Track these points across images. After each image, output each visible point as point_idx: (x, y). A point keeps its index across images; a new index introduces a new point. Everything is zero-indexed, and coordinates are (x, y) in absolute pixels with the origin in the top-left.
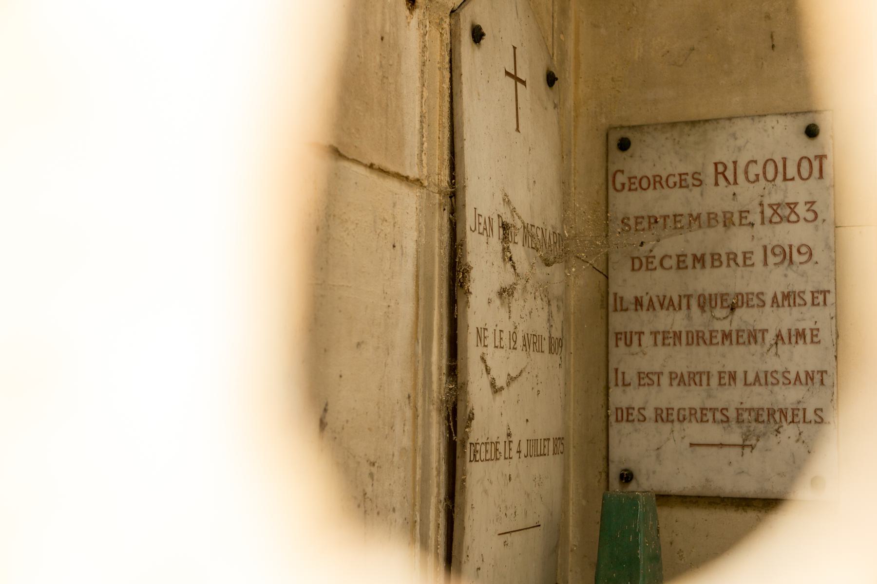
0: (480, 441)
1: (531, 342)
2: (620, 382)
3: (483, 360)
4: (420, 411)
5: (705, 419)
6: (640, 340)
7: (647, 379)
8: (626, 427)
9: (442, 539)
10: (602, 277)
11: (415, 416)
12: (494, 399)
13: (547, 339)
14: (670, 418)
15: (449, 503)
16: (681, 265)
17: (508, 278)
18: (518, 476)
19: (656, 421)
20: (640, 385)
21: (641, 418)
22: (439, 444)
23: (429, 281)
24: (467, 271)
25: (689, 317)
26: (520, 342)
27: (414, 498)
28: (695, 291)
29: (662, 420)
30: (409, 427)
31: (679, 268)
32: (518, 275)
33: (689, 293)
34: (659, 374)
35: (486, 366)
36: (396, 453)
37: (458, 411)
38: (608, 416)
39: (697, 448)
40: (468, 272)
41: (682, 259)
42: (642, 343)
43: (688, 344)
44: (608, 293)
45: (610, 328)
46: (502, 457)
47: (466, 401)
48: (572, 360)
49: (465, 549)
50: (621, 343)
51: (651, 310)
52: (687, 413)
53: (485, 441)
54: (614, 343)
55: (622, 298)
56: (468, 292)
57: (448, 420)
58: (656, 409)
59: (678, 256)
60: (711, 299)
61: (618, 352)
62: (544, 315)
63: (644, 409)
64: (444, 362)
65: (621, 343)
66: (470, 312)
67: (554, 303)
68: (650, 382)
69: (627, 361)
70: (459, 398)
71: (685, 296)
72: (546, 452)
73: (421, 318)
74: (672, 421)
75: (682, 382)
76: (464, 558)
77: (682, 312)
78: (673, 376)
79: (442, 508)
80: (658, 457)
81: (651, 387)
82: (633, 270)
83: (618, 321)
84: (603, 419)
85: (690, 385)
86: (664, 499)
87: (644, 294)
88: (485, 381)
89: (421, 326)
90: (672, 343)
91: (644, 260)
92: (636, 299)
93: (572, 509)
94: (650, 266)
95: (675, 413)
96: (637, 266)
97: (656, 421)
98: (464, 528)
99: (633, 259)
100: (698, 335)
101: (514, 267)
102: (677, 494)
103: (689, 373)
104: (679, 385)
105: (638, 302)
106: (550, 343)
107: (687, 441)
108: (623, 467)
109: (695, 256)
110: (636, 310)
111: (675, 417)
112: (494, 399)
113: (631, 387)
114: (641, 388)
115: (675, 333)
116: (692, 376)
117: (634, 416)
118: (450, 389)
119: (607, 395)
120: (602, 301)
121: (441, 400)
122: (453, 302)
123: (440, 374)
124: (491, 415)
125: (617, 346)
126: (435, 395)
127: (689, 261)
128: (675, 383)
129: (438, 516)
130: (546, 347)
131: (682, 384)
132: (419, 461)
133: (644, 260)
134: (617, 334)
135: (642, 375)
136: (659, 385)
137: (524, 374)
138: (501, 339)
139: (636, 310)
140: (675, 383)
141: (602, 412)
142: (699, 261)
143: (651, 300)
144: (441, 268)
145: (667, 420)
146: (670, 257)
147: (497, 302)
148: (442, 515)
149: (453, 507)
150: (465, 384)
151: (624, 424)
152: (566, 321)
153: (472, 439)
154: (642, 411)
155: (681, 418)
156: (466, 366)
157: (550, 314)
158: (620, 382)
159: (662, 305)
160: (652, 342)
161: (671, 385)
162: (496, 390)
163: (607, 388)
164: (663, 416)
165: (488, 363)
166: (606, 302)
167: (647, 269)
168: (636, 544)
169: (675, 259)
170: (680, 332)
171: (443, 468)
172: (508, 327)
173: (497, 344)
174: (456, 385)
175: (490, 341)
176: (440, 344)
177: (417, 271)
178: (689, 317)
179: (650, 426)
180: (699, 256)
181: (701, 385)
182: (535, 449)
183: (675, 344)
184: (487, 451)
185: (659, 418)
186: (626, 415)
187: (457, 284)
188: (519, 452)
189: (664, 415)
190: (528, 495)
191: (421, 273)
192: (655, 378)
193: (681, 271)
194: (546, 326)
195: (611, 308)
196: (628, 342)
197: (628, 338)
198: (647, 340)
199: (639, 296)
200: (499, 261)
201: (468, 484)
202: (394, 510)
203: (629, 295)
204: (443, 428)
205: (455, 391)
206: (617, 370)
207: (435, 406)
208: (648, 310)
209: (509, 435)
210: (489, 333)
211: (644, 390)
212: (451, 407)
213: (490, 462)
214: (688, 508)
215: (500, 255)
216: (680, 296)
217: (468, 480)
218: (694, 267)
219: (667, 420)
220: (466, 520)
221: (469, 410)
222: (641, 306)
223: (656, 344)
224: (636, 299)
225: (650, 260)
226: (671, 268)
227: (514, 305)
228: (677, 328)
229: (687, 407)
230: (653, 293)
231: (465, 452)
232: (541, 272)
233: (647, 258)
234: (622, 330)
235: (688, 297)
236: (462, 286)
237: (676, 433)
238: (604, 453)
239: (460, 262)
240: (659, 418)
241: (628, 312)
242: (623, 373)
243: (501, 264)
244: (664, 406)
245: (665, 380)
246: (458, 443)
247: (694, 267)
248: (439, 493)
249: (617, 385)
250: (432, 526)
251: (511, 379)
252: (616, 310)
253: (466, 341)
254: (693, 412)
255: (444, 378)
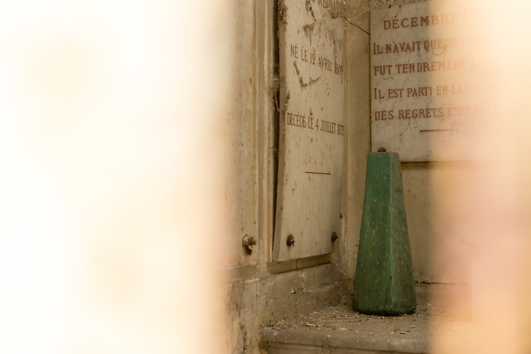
0: (294, 113)
1: (323, 63)
2: (378, 97)
3: (295, 64)
4: (257, 90)
5: (429, 115)
6: (389, 71)
7: (394, 93)
8: (382, 123)
9: (272, 171)
10: (367, 35)
11: (255, 93)
12: (302, 90)
13: (333, 64)
14: (408, 116)
15: (275, 149)
16: (414, 24)
17: (310, 21)
18: (317, 140)
19: (400, 118)
20: (389, 97)
21: (391, 117)
22: (269, 113)
23: (262, 15)
24: (284, 10)
25: (419, 55)
26: (317, 61)
27: (255, 141)
28: (423, 39)
29: (403, 117)
30: (250, 98)
31: (413, 26)
32: (315, 20)
33: (419, 40)
34: (401, 90)
35: (297, 69)
36: (243, 112)
37: (280, 94)
38: (370, 117)
39: (424, 133)
40: (285, 10)
41: (414, 20)
42: (391, 72)
43: (418, 71)
44: (370, 43)
45: (372, 64)
46: (307, 127)
47: (285, 88)
48: (349, 85)
49: (285, 176)
50: (378, 73)
51: (396, 52)
52: (418, 112)
53: (296, 114)
54: (374, 73)
55: (378, 46)
56: (285, 23)
57: (275, 100)
58: (400, 111)
59: (412, 19)
60: (432, 44)
61: (376, 78)
62: (332, 49)
63: (392, 111)
64: (272, 65)
65: (378, 73)
66: (287, 35)
67: (337, 44)
68: (396, 95)
69: (382, 83)
70: (281, 86)
71: (416, 42)
72: (333, 131)
73: (257, 34)
74: (409, 118)
75: (415, 94)
76: (285, 181)
77: (414, 52)
78: (410, 90)
79: (271, 151)
80: (401, 139)
81: (396, 98)
82: (385, 28)
83: (376, 60)
84: (368, 119)
85: (420, 95)
86: (406, 164)
87: (392, 43)
88: (296, 79)
89: (257, 40)
90: (409, 71)
91: (392, 22)
92: (387, 46)
93: (349, 174)
94: (395, 26)
95: (411, 113)
96: (387, 26)
97: (400, 118)
98: (285, 163)
99: (385, 22)
100: (424, 65)
101: (313, 14)
102: (412, 161)
103: (419, 88)
104: (413, 96)
105: (388, 48)
106: (335, 67)
107: (418, 129)
108: (380, 147)
109: (422, 18)
110: (387, 52)
111: (411, 115)
112: (302, 90)
113: (384, 99)
114: (390, 99)
115: (410, 65)
116: (421, 90)
117: (386, 116)
118: (276, 81)
119: (370, 105)
120: (367, 49)
121: (270, 88)
122: (276, 29)
123: (269, 72)
124: (299, 100)
125: (376, 75)
126: (266, 84)
127: (419, 21)
128: (411, 95)
129: (269, 156)
130: (333, 68)
131: (415, 95)
132: (257, 120)
133: (392, 22)
134: (375, 67)
135: (391, 91)
136: (401, 96)
137: (319, 80)
138: (306, 56)
139: (387, 52)
140: (411, 95)
141: (367, 115)
142: (425, 22)
143: (396, 46)
144: (269, 8)
145: (406, 118)
146: (408, 19)
147: (303, 33)
148: (272, 156)
149: (278, 151)
150: (284, 78)
151: (380, 121)
152: (345, 58)
153: (289, 111)
154: (391, 113)
155: (415, 115)
156: (285, 67)
157: (335, 50)
158: (378, 97)
159: (402, 49)
160: (397, 71)
161: (408, 96)
162: (303, 85)
163: (370, 100)
164: (404, 115)
165: (298, 67)
166: (369, 49)
167: (394, 27)
168: (388, 181)
169: (410, 20)
170: (414, 64)
171: (272, 129)
172: (310, 51)
173: (304, 58)
174: (279, 78)
175: (299, 55)
176: (269, 54)
177: (255, 6)
178: (419, 55)
179: (396, 121)
180: (425, 18)
181: (426, 95)
182: (327, 127)
183: (410, 72)
184: (298, 120)
185: (401, 116)
186: (382, 116)
187: (279, 18)
188: (317, 126)
189: (404, 115)
190: (323, 153)
191: (257, 8)
192: (399, 93)
193: (414, 28)
194: (333, 56)
195: (372, 52)
196: (382, 72)
197: (382, 70)
198: (394, 70)
199: (389, 44)
200: (304, 9)
201: (287, 137)
202: (242, 145)
203: (382, 44)
204: (272, 105)
205: (279, 82)
206: (375, 89)
207: (266, 91)
208: (394, 52)
209: (311, 114)
210: (299, 50)
211: (392, 100)
212: (276, 91)
213: (300, 127)
214: (419, 169)
215: (304, 5)
216: (413, 43)
217: (287, 134)
218: (422, 25)
219: (406, 118)
220: (286, 158)
221: (287, 93)
222: (390, 49)
223: (399, 72)
224: (387, 46)
225: (395, 22)
226: (408, 26)
227: (313, 38)
228: (411, 62)
229: (418, 109)
230: (397, 42)
231: (284, 118)
232: (331, 23)
233: (394, 21)
234: (379, 65)
235: (419, 43)
236: (282, 19)
237: (411, 125)
238: (369, 140)
239: (280, 5)
240: (401, 116)
241: (382, 54)
242: (380, 91)
243: (306, 12)
244: (404, 109)
245: (405, 93)
246: (281, 113)
247: (422, 25)
248: (269, 143)
249: (376, 98)
250: (266, 162)
251: (312, 82)
252: (375, 53)
253: (285, 52)
254: (422, 111)
255: (272, 75)
